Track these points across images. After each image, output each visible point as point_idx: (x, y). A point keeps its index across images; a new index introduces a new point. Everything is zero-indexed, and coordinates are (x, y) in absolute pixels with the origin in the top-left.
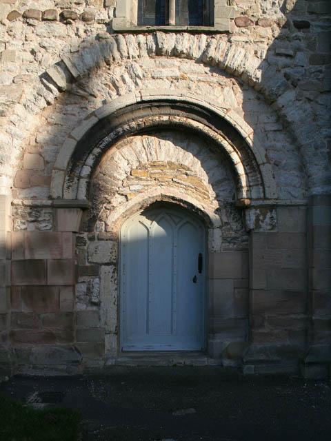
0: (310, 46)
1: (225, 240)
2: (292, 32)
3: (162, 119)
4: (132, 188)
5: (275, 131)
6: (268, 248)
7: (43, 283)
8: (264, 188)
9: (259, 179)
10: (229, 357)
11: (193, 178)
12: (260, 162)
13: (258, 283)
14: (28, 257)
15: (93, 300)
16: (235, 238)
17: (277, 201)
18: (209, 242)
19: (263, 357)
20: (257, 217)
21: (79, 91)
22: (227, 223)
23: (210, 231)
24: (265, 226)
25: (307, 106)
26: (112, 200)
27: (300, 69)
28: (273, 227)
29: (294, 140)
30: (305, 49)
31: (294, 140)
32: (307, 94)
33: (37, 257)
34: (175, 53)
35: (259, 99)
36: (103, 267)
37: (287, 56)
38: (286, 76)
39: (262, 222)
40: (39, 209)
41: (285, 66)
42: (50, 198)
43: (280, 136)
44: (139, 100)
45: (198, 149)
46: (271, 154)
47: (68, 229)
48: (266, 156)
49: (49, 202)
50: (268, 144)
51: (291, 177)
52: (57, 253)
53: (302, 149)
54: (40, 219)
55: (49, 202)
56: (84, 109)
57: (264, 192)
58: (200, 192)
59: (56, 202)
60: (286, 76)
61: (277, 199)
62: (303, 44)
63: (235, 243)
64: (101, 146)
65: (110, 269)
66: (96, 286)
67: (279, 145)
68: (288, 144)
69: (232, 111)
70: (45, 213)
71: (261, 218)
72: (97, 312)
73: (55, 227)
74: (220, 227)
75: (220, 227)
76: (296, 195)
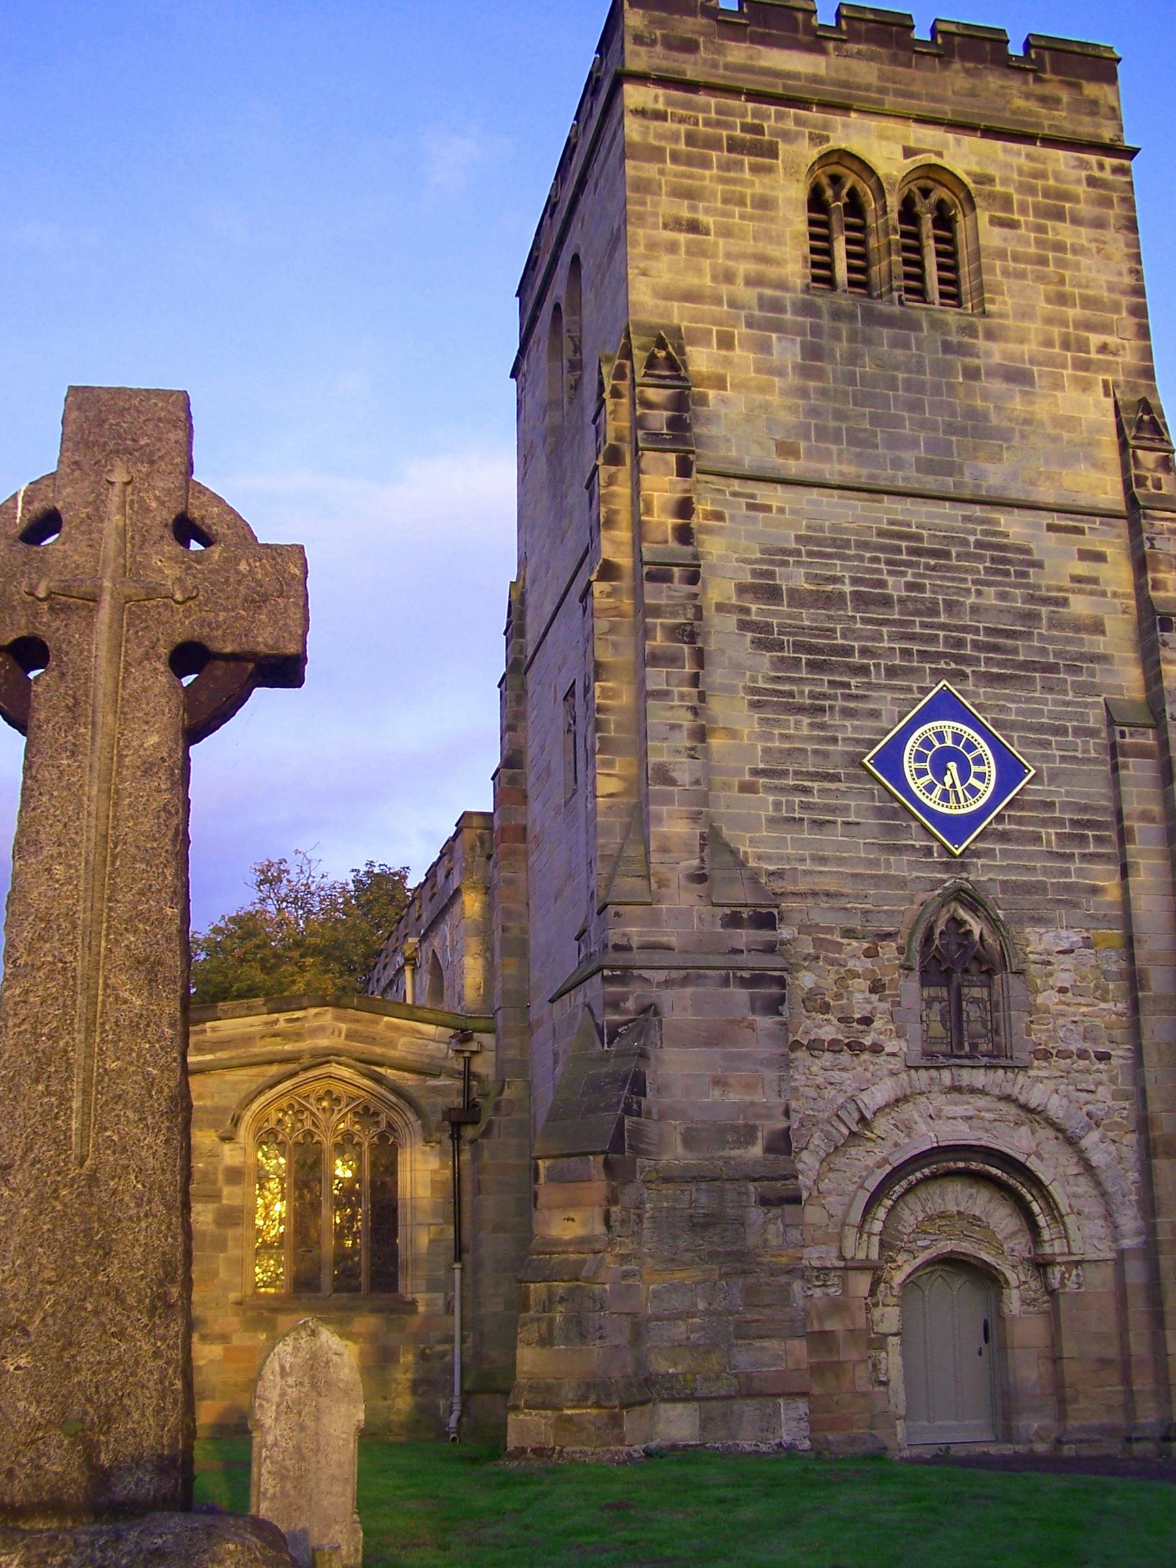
0: (1113, 1080)
1: (1023, 1301)
2: (1093, 1064)
4: (919, 1243)
7: (835, 1359)
10: (1042, 1439)
12: (1064, 1213)
13: (1069, 1348)
14: (816, 1328)
16: (1035, 1300)
19: (1082, 1436)
20: (1063, 1274)
22: (1025, 1282)
24: (1071, 1285)
25: (1112, 1148)
27: (1101, 1105)
28: (1080, 1285)
29: (1098, 1184)
31: (1098, 1184)
33: (828, 1327)
34: (973, 1091)
35: (1057, 1138)
36: (890, 1338)
37: (1088, 1091)
38: (1088, 1114)
41: (1087, 1103)
43: (1082, 1180)
44: (935, 1145)
48: (1070, 1206)
49: (842, 1264)
50: (1069, 1189)
51: (1097, 1227)
55: (842, 1264)
57: (1069, 1246)
59: (849, 1264)
60: (1088, 1114)
62: (1104, 1077)
66: (884, 1362)
67: (1080, 1190)
71: (1067, 1276)
72: (886, 1393)
73: (845, 1291)
74: (1018, 1287)
75: (1018, 1287)
76: (1101, 1247)
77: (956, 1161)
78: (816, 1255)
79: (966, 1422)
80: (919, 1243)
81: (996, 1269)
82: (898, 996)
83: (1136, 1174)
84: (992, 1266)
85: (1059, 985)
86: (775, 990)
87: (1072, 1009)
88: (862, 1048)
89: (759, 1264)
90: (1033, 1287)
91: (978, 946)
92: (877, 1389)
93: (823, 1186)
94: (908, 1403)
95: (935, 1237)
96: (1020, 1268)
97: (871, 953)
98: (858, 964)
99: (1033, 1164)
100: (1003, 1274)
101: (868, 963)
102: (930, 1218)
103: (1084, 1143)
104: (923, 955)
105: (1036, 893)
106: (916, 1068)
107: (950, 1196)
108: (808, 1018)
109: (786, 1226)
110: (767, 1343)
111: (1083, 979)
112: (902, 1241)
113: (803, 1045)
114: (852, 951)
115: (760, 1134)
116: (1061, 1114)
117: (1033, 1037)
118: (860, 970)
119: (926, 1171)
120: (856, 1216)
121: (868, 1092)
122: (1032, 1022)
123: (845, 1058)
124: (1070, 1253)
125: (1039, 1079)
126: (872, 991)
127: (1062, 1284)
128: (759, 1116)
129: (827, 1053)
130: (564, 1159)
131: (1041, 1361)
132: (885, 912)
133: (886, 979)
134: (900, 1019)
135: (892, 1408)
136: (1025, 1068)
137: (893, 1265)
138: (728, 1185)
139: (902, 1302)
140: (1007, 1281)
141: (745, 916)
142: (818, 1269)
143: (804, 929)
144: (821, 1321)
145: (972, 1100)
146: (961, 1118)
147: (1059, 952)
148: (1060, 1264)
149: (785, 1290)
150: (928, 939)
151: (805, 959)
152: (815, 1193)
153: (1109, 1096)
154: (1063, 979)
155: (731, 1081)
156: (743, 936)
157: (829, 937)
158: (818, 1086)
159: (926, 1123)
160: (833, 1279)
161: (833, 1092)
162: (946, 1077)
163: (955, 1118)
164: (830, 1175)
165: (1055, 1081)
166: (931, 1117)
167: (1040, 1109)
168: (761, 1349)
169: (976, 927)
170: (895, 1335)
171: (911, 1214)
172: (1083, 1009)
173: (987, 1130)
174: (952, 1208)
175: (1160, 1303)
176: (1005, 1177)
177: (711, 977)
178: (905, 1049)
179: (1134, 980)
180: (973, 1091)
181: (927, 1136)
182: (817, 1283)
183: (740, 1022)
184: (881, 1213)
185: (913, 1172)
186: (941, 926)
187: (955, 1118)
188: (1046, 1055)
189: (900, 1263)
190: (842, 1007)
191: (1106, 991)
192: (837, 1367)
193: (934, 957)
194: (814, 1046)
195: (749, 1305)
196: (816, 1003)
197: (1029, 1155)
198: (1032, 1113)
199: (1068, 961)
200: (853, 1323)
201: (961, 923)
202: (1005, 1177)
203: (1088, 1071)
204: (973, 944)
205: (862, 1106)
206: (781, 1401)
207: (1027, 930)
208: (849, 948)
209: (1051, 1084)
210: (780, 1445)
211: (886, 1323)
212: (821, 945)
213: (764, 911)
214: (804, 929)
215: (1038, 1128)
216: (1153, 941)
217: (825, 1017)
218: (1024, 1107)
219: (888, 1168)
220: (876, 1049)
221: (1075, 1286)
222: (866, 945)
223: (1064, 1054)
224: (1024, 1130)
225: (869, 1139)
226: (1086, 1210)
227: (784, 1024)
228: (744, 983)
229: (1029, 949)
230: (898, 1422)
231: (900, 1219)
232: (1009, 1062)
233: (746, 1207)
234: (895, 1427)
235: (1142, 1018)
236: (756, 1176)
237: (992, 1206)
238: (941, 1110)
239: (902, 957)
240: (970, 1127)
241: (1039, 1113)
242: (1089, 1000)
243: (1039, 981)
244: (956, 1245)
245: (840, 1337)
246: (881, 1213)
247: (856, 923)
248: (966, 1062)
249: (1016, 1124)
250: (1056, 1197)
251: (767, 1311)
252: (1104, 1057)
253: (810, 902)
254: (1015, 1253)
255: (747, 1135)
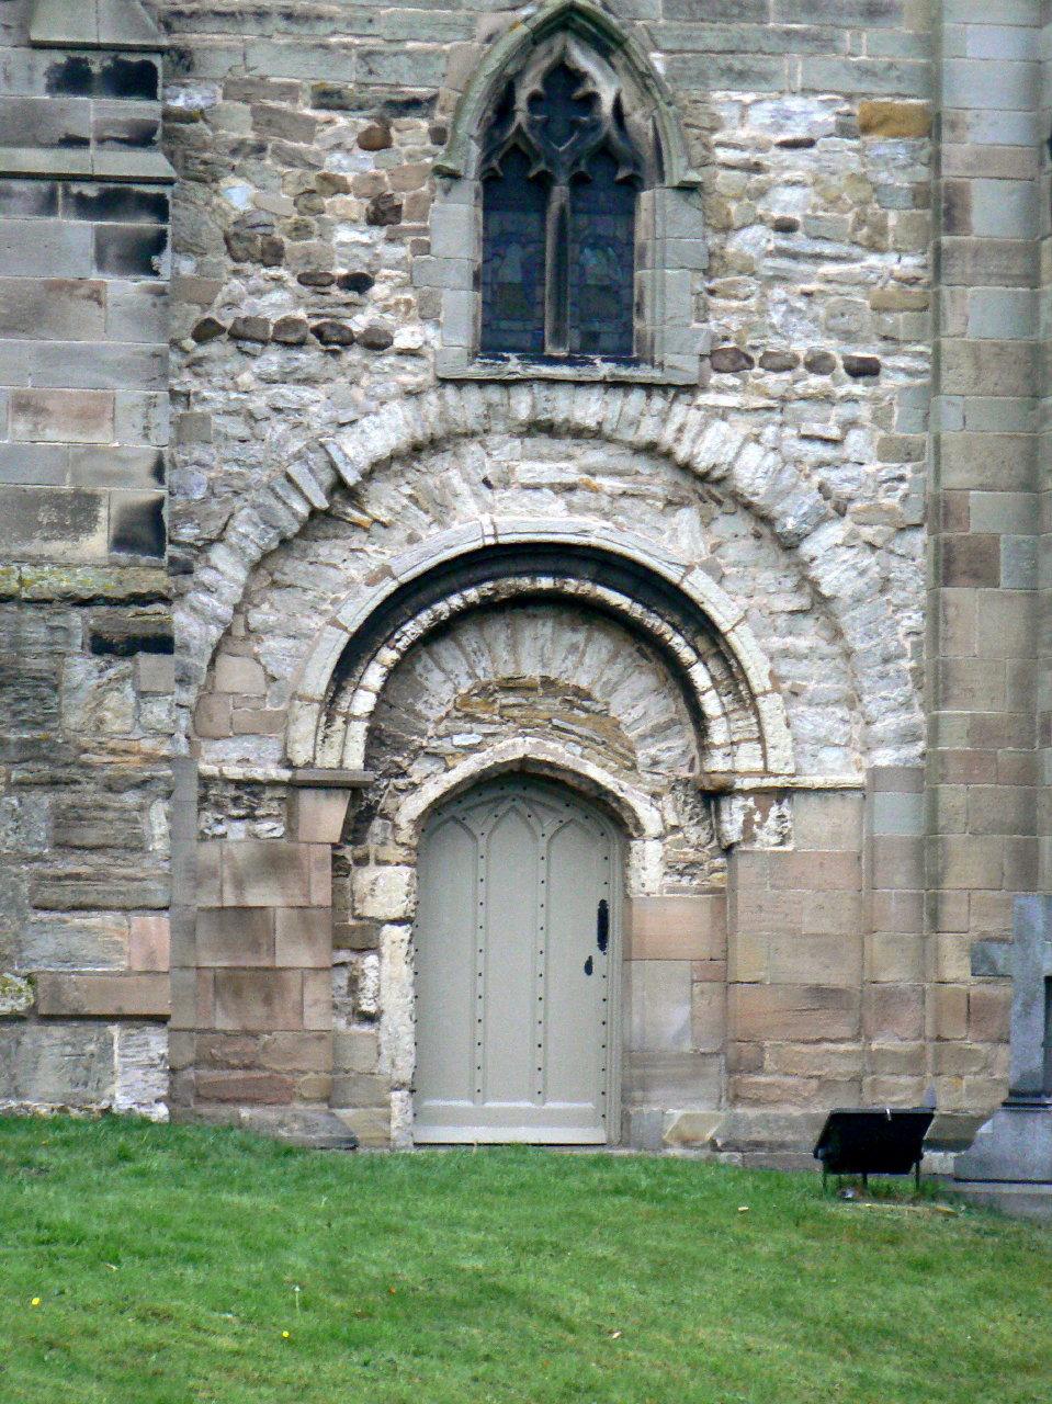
0: (881, 419)
1: (671, 868)
3: (539, 585)
4: (458, 740)
5: (792, 613)
6: (773, 886)
7: (266, 963)
8: (764, 749)
9: (755, 728)
11: (597, 718)
12: (757, 690)
14: (230, 900)
15: (364, 1008)
16: (693, 864)
17: (793, 780)
18: (630, 873)
21: (350, 510)
22: (676, 828)
23: (636, 845)
24: (766, 839)
25: (869, 560)
26: (410, 770)
30: (869, 424)
32: (868, 533)
33: (254, 898)
35: (758, 536)
36: (387, 926)
37: (826, 441)
38: (821, 488)
39: (760, 826)
40: (256, 789)
41: (822, 464)
42: (288, 764)
44: (490, 541)
45: (611, 647)
46: (784, 668)
47: (321, 839)
49: (286, 775)
50: (776, 643)
52: (297, 891)
53: (854, 658)
54: (257, 813)
56: (361, 555)
57: (764, 756)
58: (615, 752)
59: (302, 775)
61: (793, 775)
62: (864, 412)
63: (693, 876)
64: (400, 645)
65: (401, 933)
66: (372, 974)
67: (802, 644)
68: (823, 644)
69: (697, 569)
70: (271, 799)
71: (757, 817)
74: (660, 837)
75: (660, 837)
77: (534, 574)
78: (235, 756)
79: (550, 1105)
80: (458, 740)
81: (618, 799)
82: (425, 231)
83: (917, 617)
84: (609, 793)
85: (776, 214)
86: (146, 224)
87: (804, 267)
88: (348, 341)
89: (85, 766)
90: (693, 839)
91: (609, 125)
92: (355, 1028)
93: (256, 618)
94: (419, 1055)
95: (492, 729)
96: (667, 799)
97: (375, 142)
98: (345, 163)
99: (699, 587)
100: (632, 810)
101: (368, 162)
102: (484, 690)
103: (808, 548)
104: (490, 141)
105: (741, 16)
106: (460, 383)
107: (528, 647)
108: (236, 273)
109: (142, 694)
110: (94, 920)
111: (833, 202)
112: (422, 734)
113: (222, 330)
114: (336, 134)
115: (103, 513)
116: (762, 486)
117: (713, 323)
118: (350, 177)
119: (472, 594)
120: (318, 679)
121: (357, 429)
122: (712, 292)
123: (310, 359)
124: (766, 773)
125: (723, 414)
126: (375, 219)
127: (748, 833)
128: (106, 477)
129: (273, 347)
130: (305, 489)
131: (697, 989)
132: (409, 54)
133: (403, 198)
134: (427, 286)
135: (385, 1066)
136: (691, 389)
137: (401, 783)
138: (30, 613)
139: (420, 857)
140: (639, 827)
141: (95, 69)
142: (239, 784)
143: (240, 89)
144: (239, 884)
145: (577, 452)
146: (552, 486)
147: (785, 145)
148: (742, 792)
149: (130, 819)
150: (503, 107)
151: (234, 152)
152: (240, 632)
153: (871, 451)
154: (788, 202)
155: (51, 404)
156: (92, 111)
157: (285, 105)
158: (251, 415)
159: (476, 495)
160: (269, 804)
161: (281, 428)
162: (522, 405)
163: (537, 488)
164: (275, 595)
165: (754, 418)
166: (486, 482)
167: (717, 474)
168: (81, 930)
169: (607, 87)
170: (394, 922)
171: (447, 681)
172: (830, 269)
173: (606, 516)
174: (532, 671)
175: (936, 880)
176: (637, 610)
177: (21, 194)
178: (437, 345)
179: (942, 207)
180: (579, 433)
181: (474, 524)
182: (235, 812)
183: (73, 286)
184: (374, 676)
185: (444, 596)
186: (531, 84)
187: (537, 488)
188: (738, 361)
189: (415, 779)
190: (307, 257)
191: (880, 229)
192: (268, 983)
193: (515, 148)
194: (245, 335)
195: (63, 846)
196: (254, 246)
197: (689, 568)
198: (706, 487)
199: (801, 164)
200: (307, 895)
201: (578, 77)
202: (643, 613)
203: (827, 399)
204: (596, 126)
205: (337, 457)
206: (115, 1030)
207: (718, 95)
208: (329, 130)
209: (743, 426)
210: (107, 1112)
211: (381, 898)
212: (269, 123)
213: (135, 59)
214: (240, 89)
215: (717, 511)
216: (989, 120)
217: (273, 272)
218: (686, 468)
219: (390, 586)
220: (376, 343)
221: (775, 839)
222: (364, 124)
223: (784, 364)
224: (687, 518)
225: (356, 525)
226: (812, 686)
227: (160, 292)
228: (84, 206)
229: (717, 137)
230: (396, 1095)
231: (420, 690)
232: (655, 375)
233: (63, 655)
234: (387, 1104)
235: (946, 291)
236: (86, 595)
237: (618, 667)
238: (511, 470)
239: (441, 151)
240: (570, 507)
241: (719, 481)
242: (843, 249)
243: (733, 207)
244: (536, 747)
245: (281, 919)
246: (374, 676)
247: (345, 77)
248: (565, 372)
249: (669, 503)
250: (743, 656)
251: (95, 858)
252: (864, 370)
253: (251, 31)
254: (661, 769)
255: (78, 511)
